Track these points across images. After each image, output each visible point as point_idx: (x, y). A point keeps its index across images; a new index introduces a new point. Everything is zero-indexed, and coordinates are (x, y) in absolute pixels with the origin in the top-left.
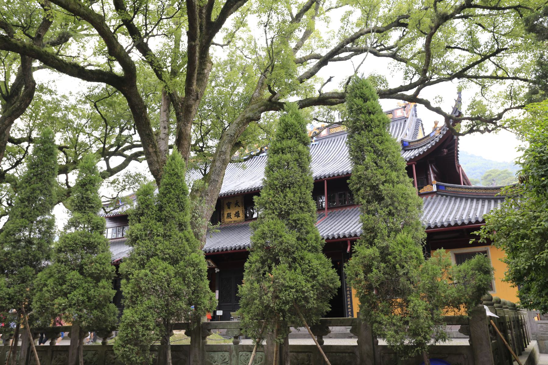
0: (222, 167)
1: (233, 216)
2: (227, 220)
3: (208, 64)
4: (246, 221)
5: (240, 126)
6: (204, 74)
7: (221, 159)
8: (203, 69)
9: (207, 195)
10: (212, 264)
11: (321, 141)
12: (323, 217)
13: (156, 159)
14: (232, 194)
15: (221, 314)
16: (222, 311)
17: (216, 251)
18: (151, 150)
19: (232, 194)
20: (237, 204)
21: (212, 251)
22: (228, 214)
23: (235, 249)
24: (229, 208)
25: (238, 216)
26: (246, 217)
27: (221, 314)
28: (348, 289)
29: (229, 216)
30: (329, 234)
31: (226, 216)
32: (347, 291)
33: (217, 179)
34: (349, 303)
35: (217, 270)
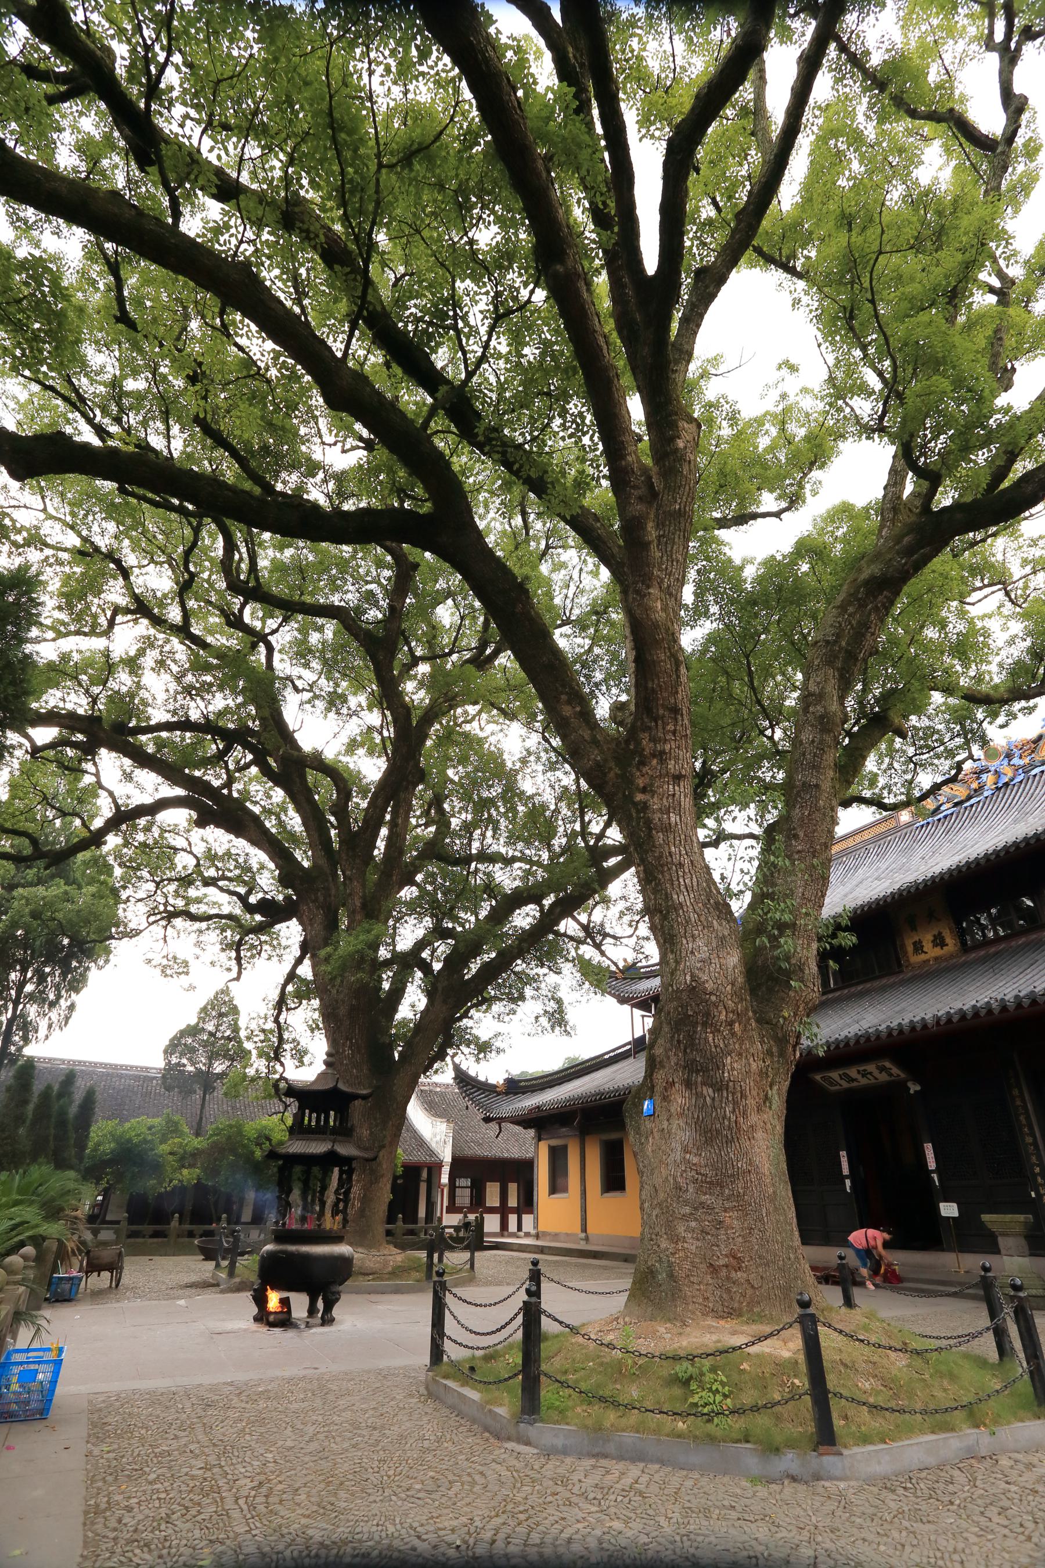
1: (928, 946)
2: (916, 959)
3: (683, 424)
5: (851, 609)
6: (677, 450)
7: (810, 717)
8: (672, 439)
9: (796, 837)
10: (895, 1071)
13: (586, 734)
14: (912, 890)
17: (895, 1033)
18: (567, 711)
20: (931, 917)
21: (884, 1035)
22: (914, 944)
24: (914, 928)
25: (943, 944)
26: (963, 943)
29: (918, 947)
31: (910, 949)
33: (814, 781)
35: (914, 1088)
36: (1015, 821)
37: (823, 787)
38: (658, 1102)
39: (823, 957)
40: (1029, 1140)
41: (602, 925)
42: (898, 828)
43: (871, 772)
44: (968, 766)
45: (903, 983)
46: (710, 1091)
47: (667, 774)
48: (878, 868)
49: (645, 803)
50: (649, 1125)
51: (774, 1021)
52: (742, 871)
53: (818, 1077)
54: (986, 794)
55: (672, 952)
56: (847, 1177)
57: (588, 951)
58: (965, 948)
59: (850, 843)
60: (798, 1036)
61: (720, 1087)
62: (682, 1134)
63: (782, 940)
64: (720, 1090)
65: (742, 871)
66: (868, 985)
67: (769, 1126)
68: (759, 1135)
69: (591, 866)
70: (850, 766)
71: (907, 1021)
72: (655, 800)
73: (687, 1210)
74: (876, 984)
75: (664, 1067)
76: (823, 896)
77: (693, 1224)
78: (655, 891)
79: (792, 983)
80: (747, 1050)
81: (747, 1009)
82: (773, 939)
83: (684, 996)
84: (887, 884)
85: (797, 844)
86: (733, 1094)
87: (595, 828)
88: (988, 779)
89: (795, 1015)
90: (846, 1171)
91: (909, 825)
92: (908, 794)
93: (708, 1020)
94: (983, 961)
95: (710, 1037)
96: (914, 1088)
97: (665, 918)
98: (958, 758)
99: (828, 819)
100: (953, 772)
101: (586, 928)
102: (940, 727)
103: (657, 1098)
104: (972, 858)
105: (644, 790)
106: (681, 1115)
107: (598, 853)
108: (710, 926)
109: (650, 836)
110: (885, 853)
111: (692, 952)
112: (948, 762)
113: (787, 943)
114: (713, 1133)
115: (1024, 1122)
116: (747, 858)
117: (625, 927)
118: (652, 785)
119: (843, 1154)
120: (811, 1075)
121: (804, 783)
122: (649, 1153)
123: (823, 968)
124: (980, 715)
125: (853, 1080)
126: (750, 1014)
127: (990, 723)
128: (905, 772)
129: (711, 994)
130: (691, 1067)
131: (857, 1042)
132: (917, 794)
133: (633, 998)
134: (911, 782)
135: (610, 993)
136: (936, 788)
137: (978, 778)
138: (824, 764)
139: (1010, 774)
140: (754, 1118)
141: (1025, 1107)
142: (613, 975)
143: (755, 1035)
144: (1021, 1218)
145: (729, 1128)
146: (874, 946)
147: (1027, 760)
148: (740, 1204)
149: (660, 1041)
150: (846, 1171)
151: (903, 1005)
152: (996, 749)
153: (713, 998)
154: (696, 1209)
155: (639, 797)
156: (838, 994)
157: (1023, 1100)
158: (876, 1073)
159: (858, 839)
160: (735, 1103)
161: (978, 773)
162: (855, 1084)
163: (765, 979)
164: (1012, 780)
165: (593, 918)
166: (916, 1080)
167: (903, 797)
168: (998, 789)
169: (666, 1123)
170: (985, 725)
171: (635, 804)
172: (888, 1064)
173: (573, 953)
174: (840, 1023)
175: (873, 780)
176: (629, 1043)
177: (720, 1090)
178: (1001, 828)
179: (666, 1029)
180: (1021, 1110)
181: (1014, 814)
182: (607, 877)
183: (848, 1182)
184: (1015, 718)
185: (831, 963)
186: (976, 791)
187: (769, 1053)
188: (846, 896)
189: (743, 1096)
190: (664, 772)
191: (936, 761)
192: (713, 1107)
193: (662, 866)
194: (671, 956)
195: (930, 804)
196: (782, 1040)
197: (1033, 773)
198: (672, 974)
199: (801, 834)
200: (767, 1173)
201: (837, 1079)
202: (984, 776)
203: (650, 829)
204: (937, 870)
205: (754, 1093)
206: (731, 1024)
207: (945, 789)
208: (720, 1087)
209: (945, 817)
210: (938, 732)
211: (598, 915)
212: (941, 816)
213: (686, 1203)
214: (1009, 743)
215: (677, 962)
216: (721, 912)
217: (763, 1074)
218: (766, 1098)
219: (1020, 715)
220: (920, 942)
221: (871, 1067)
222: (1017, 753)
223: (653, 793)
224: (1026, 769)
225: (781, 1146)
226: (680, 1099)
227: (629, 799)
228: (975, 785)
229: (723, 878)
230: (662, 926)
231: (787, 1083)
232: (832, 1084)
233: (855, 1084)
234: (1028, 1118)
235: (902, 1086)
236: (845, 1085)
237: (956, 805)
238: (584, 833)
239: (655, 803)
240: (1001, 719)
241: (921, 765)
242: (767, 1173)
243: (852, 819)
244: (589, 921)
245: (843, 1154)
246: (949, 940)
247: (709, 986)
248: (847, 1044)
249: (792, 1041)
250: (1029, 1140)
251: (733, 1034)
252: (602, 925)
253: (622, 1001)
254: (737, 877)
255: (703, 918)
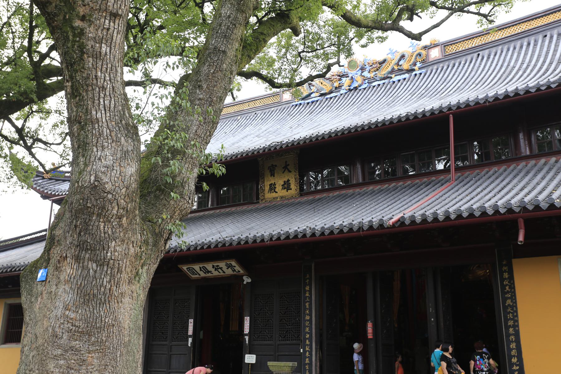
0: (236, 18)
1: (279, 188)
2: (269, 196)
4: (301, 195)
10: (238, 268)
11: (431, 68)
12: (448, 184)
15: (254, 361)
16: (254, 356)
17: (242, 243)
19: (278, 148)
20: (286, 168)
21: (235, 244)
22: (271, 185)
23: (279, 239)
24: (273, 175)
25: (288, 188)
26: (301, 189)
27: (254, 361)
28: (511, 323)
29: (272, 188)
30: (475, 207)
32: (507, 327)
34: (514, 352)
35: (247, 280)
36: (354, 114)
37: (229, 54)
38: (51, 271)
39: (201, 178)
40: (308, 318)
41: (36, 132)
42: (280, 103)
43: (271, 57)
44: (335, 69)
45: (256, 210)
46: (94, 265)
47: (106, 10)
48: (260, 129)
49: (82, 30)
50: (40, 288)
51: (155, 220)
52: (153, 104)
53: (185, 268)
54: (342, 92)
55: (83, 156)
56: (190, 336)
57: (20, 151)
58: (302, 192)
59: (245, 107)
60: (171, 233)
61: (102, 263)
62: (65, 295)
63: (171, 162)
64: (102, 265)
65: (153, 104)
66: (234, 209)
67: (135, 295)
68: (126, 300)
69: (33, 80)
70: (253, 45)
71: (252, 235)
72: (92, 29)
73: (59, 352)
74: (239, 209)
75: (60, 245)
76: (211, 135)
77: (62, 362)
78: (78, 105)
79: (172, 194)
80: (129, 238)
81: (135, 208)
82: (166, 160)
83: (87, 191)
84: (263, 141)
85: (201, 94)
86: (112, 269)
87: (43, 49)
88: (346, 81)
89: (171, 217)
90: (190, 332)
91: (288, 102)
92: (292, 79)
93: (102, 213)
94: (311, 203)
95: (102, 225)
96: (247, 280)
97: (82, 128)
98: (331, 61)
99: (227, 79)
100: (324, 70)
101: (20, 131)
102: (324, 36)
103: (51, 268)
104: (321, 133)
105: (83, 18)
106: (67, 282)
107: (40, 72)
108: (118, 141)
109: (82, 59)
110: (267, 119)
111: (100, 159)
112: (323, 63)
113: (175, 165)
114: (90, 296)
115: (307, 307)
116: (159, 95)
117: (57, 137)
118: (91, 16)
119: (191, 321)
120: (180, 266)
121: (215, 48)
122: (36, 309)
123: (198, 189)
124: (351, 35)
125: (209, 272)
126: (137, 212)
127: (357, 42)
128: (294, 63)
129: (109, 193)
130: (82, 246)
131: (216, 246)
132: (298, 80)
133: (55, 196)
134: (295, 71)
135: (35, 189)
136: (311, 78)
137: (340, 80)
138: (234, 36)
139: (360, 82)
140: (125, 288)
141: (310, 298)
142: (39, 175)
143: (138, 228)
144: (290, 364)
145: (104, 293)
146: (240, 180)
147: (372, 75)
148: (102, 348)
149: (62, 225)
150: (190, 332)
151: (253, 225)
152: (356, 62)
153: (110, 196)
154: (66, 351)
155: (78, 23)
156: (212, 212)
157: (311, 294)
158: (225, 268)
159: (252, 105)
160: (112, 276)
161: (341, 76)
162: (210, 275)
163: (153, 188)
164: (360, 86)
165: (27, 124)
166: (249, 276)
167: (287, 81)
168: (350, 90)
169: (54, 287)
170: (353, 42)
171: (73, 28)
172: (234, 263)
173: (6, 151)
174: (208, 232)
175: (271, 63)
176: (45, 230)
177: (102, 265)
178: (344, 117)
179: (68, 215)
180: (308, 300)
181: (354, 109)
182: (45, 93)
183: (190, 340)
184: (372, 42)
185: (205, 184)
186: (336, 88)
187: (146, 242)
188: (233, 144)
189: (119, 271)
190: (103, 7)
191: (315, 60)
192: (95, 277)
193: (87, 86)
194: (82, 159)
195: (305, 90)
196: (160, 235)
197: (374, 84)
198: (80, 173)
199: (205, 86)
200: (126, 327)
201: (197, 271)
202: (344, 79)
203: (83, 53)
204: (297, 137)
205: (128, 270)
206: (120, 218)
207: (317, 81)
208: (102, 263)
209: (313, 102)
210: (322, 39)
211: (33, 123)
212: (310, 101)
213: (59, 347)
214: (365, 60)
215: (86, 165)
216: (129, 132)
217: (138, 257)
218: (137, 273)
219: (376, 41)
220: (275, 184)
221: (222, 264)
222: (368, 68)
223: (91, 23)
224: (371, 81)
225: (142, 309)
226: (69, 270)
227: (68, 22)
228: (336, 84)
229: (138, 107)
230: (79, 134)
231: (156, 266)
232: (193, 274)
233: (210, 275)
234: (310, 305)
235: (239, 278)
236: (202, 274)
237: (322, 95)
238: (30, 50)
239: (91, 32)
240: (364, 41)
241: (305, 60)
242: (126, 327)
243: (250, 89)
244: (23, 126)
245: (191, 321)
246: (293, 186)
247: (108, 187)
248: (209, 247)
249: (165, 236)
250: (308, 318)
251: (121, 225)
252: (36, 132)
253: (45, 196)
254: (149, 108)
255: (113, 134)
